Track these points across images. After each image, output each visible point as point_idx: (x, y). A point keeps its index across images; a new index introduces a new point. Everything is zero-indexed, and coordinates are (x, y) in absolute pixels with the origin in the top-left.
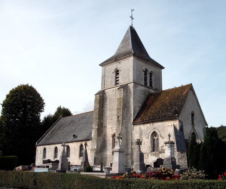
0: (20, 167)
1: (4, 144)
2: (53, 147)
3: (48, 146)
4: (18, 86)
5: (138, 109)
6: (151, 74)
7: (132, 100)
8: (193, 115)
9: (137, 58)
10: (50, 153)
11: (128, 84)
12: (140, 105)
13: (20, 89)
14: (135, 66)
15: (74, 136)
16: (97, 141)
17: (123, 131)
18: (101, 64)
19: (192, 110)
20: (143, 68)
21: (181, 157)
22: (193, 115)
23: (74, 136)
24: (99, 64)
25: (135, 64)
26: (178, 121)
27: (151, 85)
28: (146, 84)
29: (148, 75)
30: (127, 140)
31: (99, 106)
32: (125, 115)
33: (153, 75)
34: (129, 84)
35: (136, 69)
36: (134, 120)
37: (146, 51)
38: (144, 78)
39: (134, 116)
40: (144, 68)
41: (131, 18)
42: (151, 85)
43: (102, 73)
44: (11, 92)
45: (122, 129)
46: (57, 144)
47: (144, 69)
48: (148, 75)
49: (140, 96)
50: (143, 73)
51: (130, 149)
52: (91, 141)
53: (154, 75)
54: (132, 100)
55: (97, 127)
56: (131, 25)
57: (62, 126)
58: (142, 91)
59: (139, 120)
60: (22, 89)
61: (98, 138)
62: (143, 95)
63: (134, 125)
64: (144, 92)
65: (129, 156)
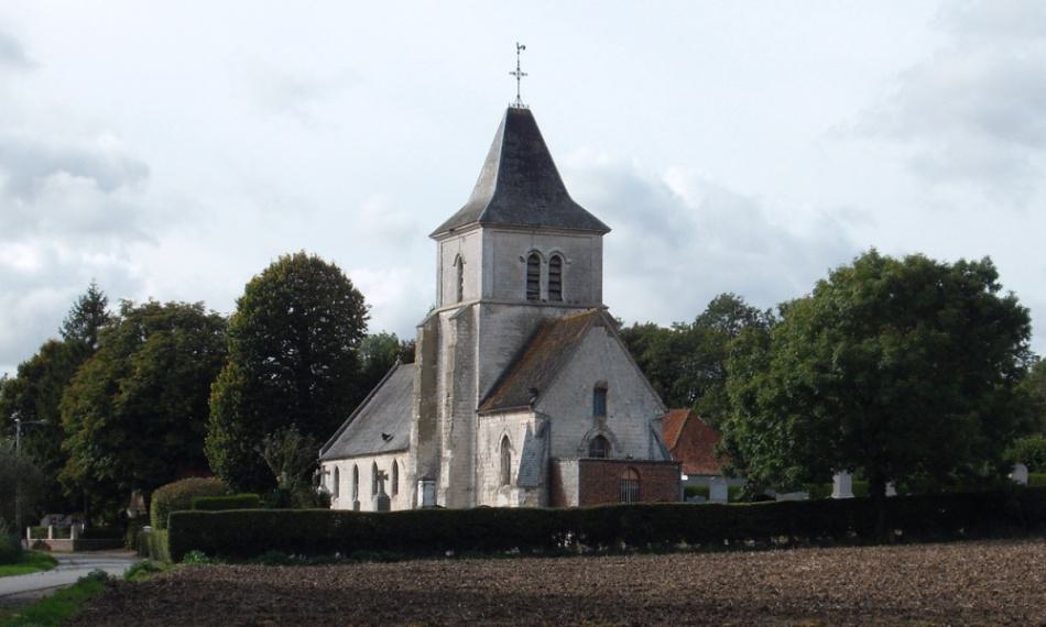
0: (752, 542)
2: (350, 463)
3: (341, 462)
4: (254, 280)
5: (496, 373)
8: (601, 392)
10: (346, 482)
11: (472, 305)
12: (504, 360)
13: (273, 280)
14: (490, 254)
16: (418, 453)
18: (434, 234)
20: (523, 252)
22: (601, 392)
23: (385, 437)
26: (534, 415)
27: (555, 290)
28: (533, 296)
30: (469, 453)
32: (463, 389)
35: (490, 264)
36: (481, 404)
37: (562, 186)
38: (524, 278)
39: (481, 391)
40: (528, 249)
42: (555, 290)
43: (11, 591)
44: (250, 289)
45: (452, 427)
46: (380, 454)
47: (525, 254)
48: (544, 269)
49: (505, 336)
50: (523, 267)
51: (474, 475)
52: (408, 454)
53: (569, 260)
57: (389, 395)
60: (281, 278)
62: (516, 329)
63: (480, 415)
64: (522, 321)
65: (472, 493)
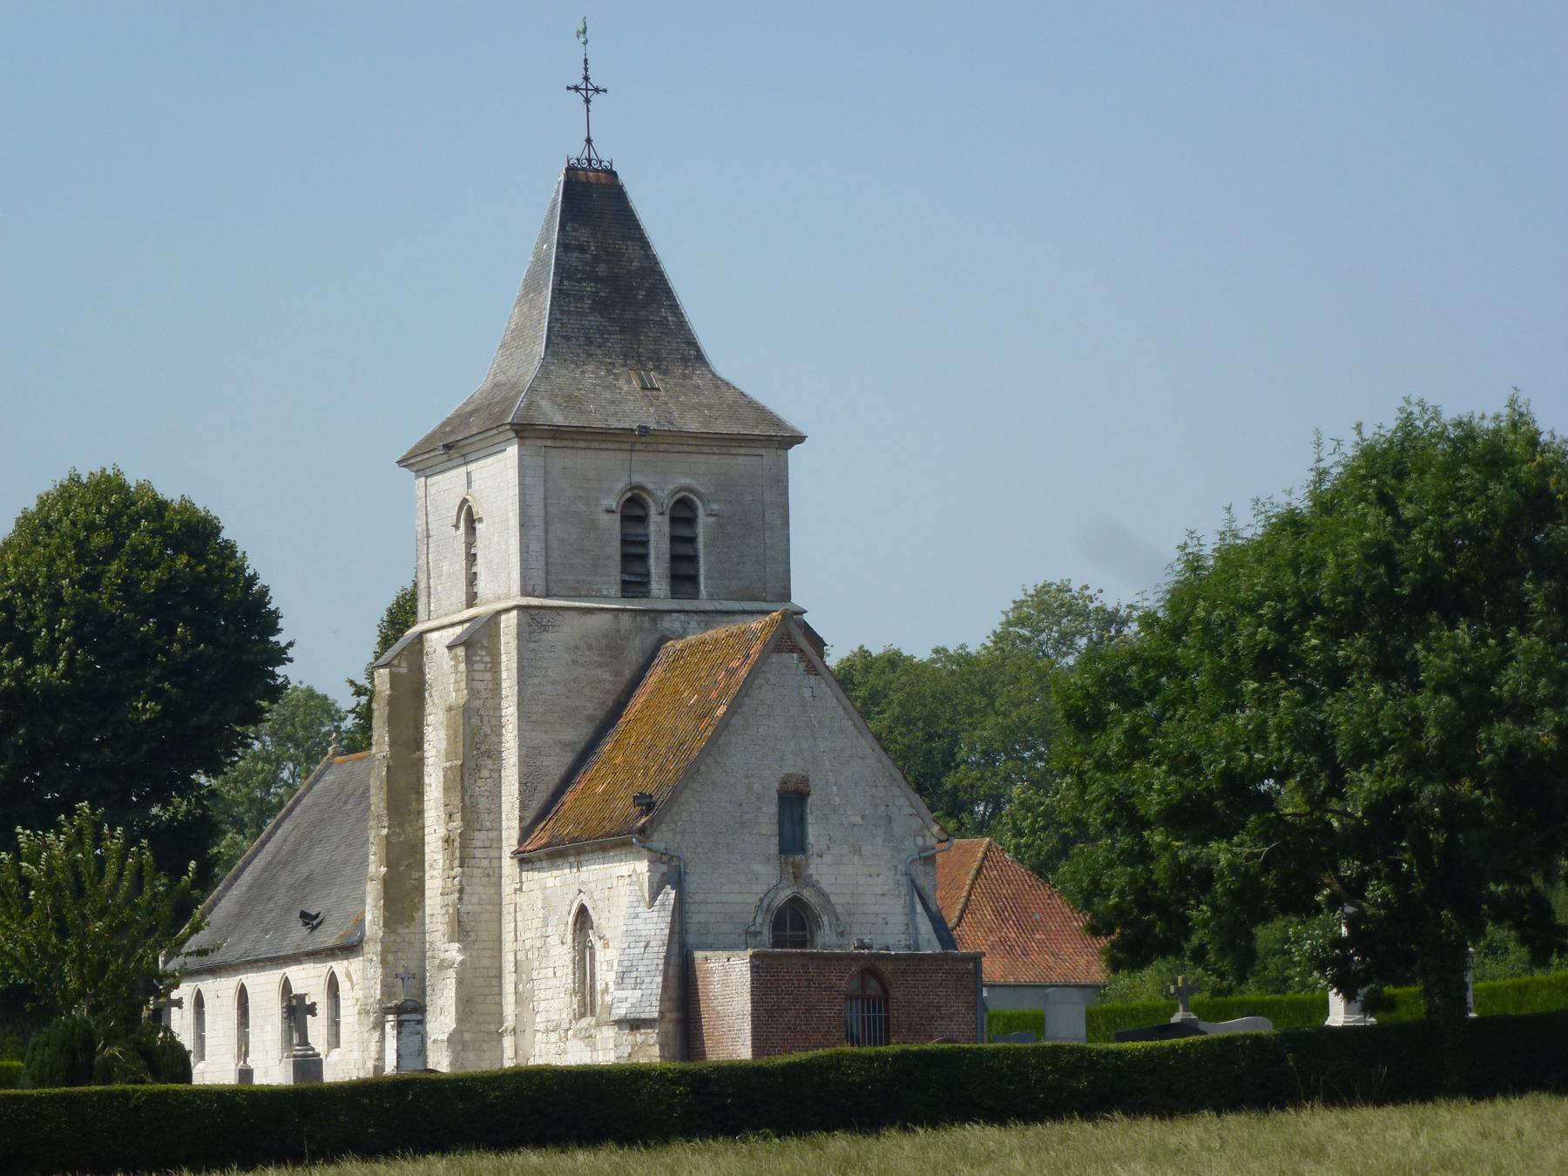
1: (1168, 715)
5: (555, 765)
6: (683, 512)
7: (510, 711)
9: (549, 443)
11: (499, 613)
15: (304, 915)
17: (475, 899)
19: (788, 770)
21: (629, 1050)
22: (793, 800)
23: (304, 915)
24: (398, 459)
25: (528, 481)
29: (658, 529)
31: (391, 745)
33: (701, 511)
34: (429, 636)
39: (523, 807)
41: (578, 98)
48: (658, 529)
54: (510, 711)
55: (383, 870)
56: (577, 151)
58: (590, 647)
59: (558, 828)
61: (392, 937)
62: (600, 665)
